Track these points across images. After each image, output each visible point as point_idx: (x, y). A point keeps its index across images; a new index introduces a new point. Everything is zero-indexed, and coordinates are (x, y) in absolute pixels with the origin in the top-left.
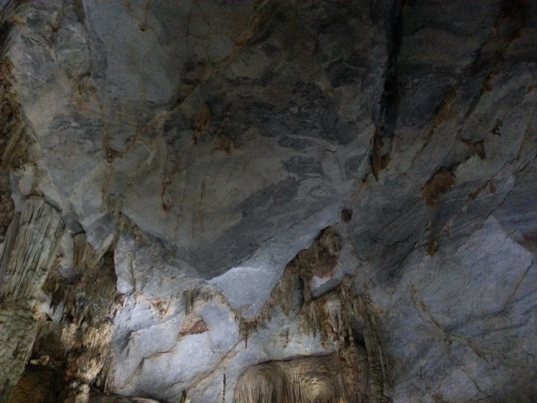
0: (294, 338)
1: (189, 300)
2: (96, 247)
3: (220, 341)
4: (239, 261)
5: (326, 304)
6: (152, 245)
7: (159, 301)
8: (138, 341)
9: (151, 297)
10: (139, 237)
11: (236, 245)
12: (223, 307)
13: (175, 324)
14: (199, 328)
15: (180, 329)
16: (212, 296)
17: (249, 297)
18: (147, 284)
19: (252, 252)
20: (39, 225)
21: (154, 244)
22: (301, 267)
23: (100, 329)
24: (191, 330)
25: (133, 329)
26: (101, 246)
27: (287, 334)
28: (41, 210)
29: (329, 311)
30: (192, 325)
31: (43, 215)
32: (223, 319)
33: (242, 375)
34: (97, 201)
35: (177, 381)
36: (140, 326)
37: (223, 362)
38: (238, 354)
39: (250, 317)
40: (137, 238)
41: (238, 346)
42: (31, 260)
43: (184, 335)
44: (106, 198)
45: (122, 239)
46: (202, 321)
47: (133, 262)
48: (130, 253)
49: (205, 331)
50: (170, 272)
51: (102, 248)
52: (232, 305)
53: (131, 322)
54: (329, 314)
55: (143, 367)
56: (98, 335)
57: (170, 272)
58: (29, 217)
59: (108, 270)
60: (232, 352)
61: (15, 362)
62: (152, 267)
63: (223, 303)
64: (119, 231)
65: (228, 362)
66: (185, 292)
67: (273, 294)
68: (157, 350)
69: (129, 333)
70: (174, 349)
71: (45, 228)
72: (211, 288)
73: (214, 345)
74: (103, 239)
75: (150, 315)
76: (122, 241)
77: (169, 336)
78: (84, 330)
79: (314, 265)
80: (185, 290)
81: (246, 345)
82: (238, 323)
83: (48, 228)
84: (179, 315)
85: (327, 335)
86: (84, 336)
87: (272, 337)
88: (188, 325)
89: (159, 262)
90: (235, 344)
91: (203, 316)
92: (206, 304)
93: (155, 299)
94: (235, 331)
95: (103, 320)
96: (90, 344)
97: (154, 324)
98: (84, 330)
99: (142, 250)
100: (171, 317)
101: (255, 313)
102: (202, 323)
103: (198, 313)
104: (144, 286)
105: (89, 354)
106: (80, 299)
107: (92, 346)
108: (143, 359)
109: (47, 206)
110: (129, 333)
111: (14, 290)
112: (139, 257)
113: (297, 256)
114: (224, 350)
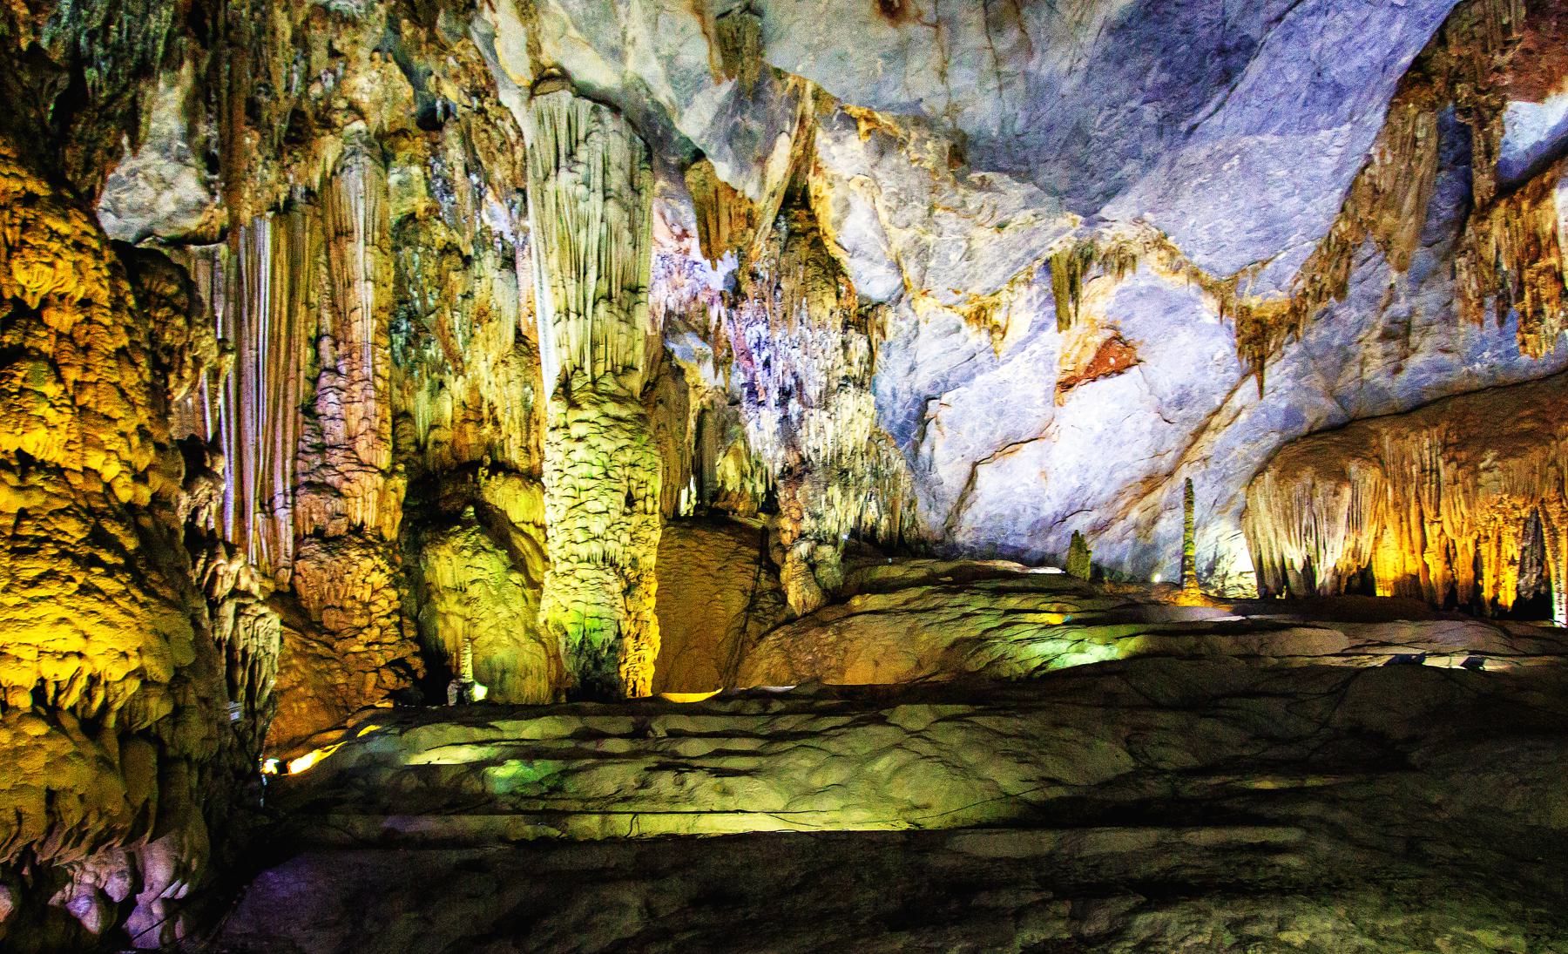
0: (1428, 340)
1: (1066, 281)
2: (751, 190)
3: (1182, 386)
4: (1184, 127)
5: (1548, 202)
6: (909, 136)
7: (977, 303)
8: (951, 424)
9: (953, 298)
10: (867, 120)
11: (1164, 67)
12: (1178, 284)
13: (1038, 360)
14: (1112, 361)
15: (1057, 376)
16: (1134, 257)
17: (1261, 234)
18: (932, 263)
19: (1227, 78)
20: (581, 169)
21: (914, 135)
22: (1454, 78)
23: (832, 409)
24: (1088, 370)
25: (931, 393)
26: (763, 182)
27: (1408, 329)
28: (573, 122)
29: (1555, 223)
30: (1089, 356)
31: (581, 135)
32: (1183, 323)
33: (1261, 471)
34: (698, 53)
35: (1074, 509)
36: (945, 382)
37: (1197, 445)
38: (1243, 417)
39: (1267, 299)
40: (863, 126)
41: (1239, 393)
42: (592, 274)
43: (1070, 386)
44: (712, 31)
45: (825, 141)
46: (1118, 338)
47: (878, 205)
48: (863, 178)
49: (1129, 366)
50: (987, 211)
51: (769, 189)
52: (1204, 273)
53: (920, 377)
54: (1554, 235)
55: (978, 484)
56: (829, 426)
57: (987, 211)
58: (553, 153)
59: (802, 250)
60: (1224, 412)
61: (636, 520)
62: (932, 209)
63: (1176, 272)
64: (802, 119)
65: (1210, 443)
66: (1048, 262)
67: (1349, 204)
68: (1006, 439)
69: (924, 403)
70: (1050, 429)
71: (599, 173)
72: (1126, 232)
73: (1166, 400)
74: (762, 161)
75: (965, 348)
76: (828, 147)
77: (1029, 398)
78: (795, 418)
79: (1509, 55)
80: (1049, 254)
81: (1261, 387)
82: (1233, 324)
83: (605, 172)
84: (1044, 335)
85: (1542, 312)
86: (799, 433)
87: (1352, 349)
88: (1079, 358)
89: (946, 186)
90: (1228, 387)
91: (1120, 325)
92: (1120, 286)
93: (966, 301)
94: (1228, 350)
95: (835, 385)
96: (817, 451)
97: (982, 371)
98: (795, 418)
99: (891, 161)
100: (1023, 345)
101: (1287, 282)
102: (1118, 346)
103: (1100, 317)
104: (926, 269)
105: (819, 474)
106: (757, 345)
107: (822, 454)
108: (975, 464)
109: (585, 105)
110: (924, 403)
111: (582, 358)
112: (889, 184)
113: (1441, 38)
114: (1200, 412)
